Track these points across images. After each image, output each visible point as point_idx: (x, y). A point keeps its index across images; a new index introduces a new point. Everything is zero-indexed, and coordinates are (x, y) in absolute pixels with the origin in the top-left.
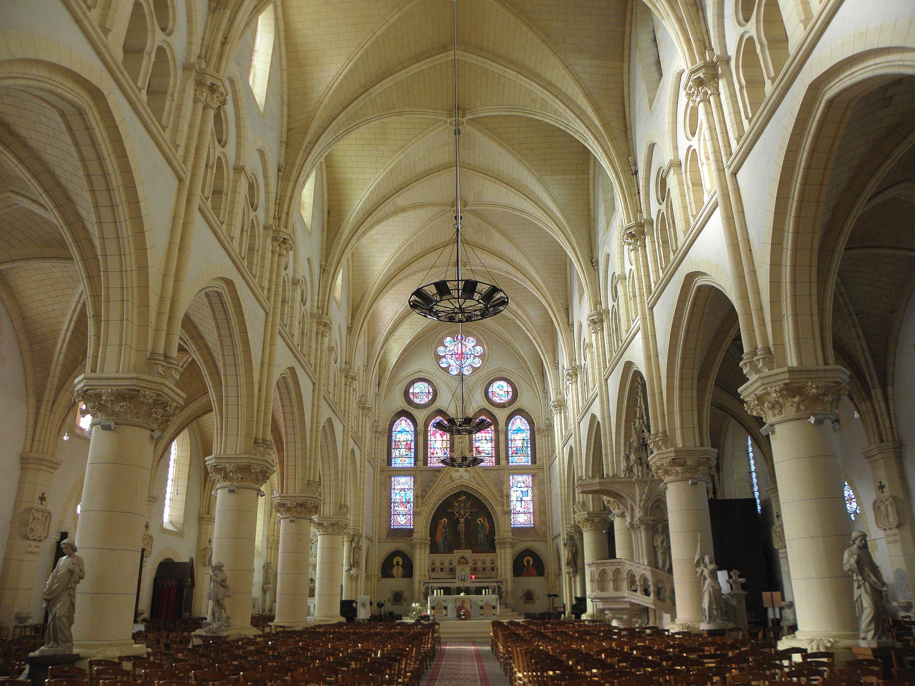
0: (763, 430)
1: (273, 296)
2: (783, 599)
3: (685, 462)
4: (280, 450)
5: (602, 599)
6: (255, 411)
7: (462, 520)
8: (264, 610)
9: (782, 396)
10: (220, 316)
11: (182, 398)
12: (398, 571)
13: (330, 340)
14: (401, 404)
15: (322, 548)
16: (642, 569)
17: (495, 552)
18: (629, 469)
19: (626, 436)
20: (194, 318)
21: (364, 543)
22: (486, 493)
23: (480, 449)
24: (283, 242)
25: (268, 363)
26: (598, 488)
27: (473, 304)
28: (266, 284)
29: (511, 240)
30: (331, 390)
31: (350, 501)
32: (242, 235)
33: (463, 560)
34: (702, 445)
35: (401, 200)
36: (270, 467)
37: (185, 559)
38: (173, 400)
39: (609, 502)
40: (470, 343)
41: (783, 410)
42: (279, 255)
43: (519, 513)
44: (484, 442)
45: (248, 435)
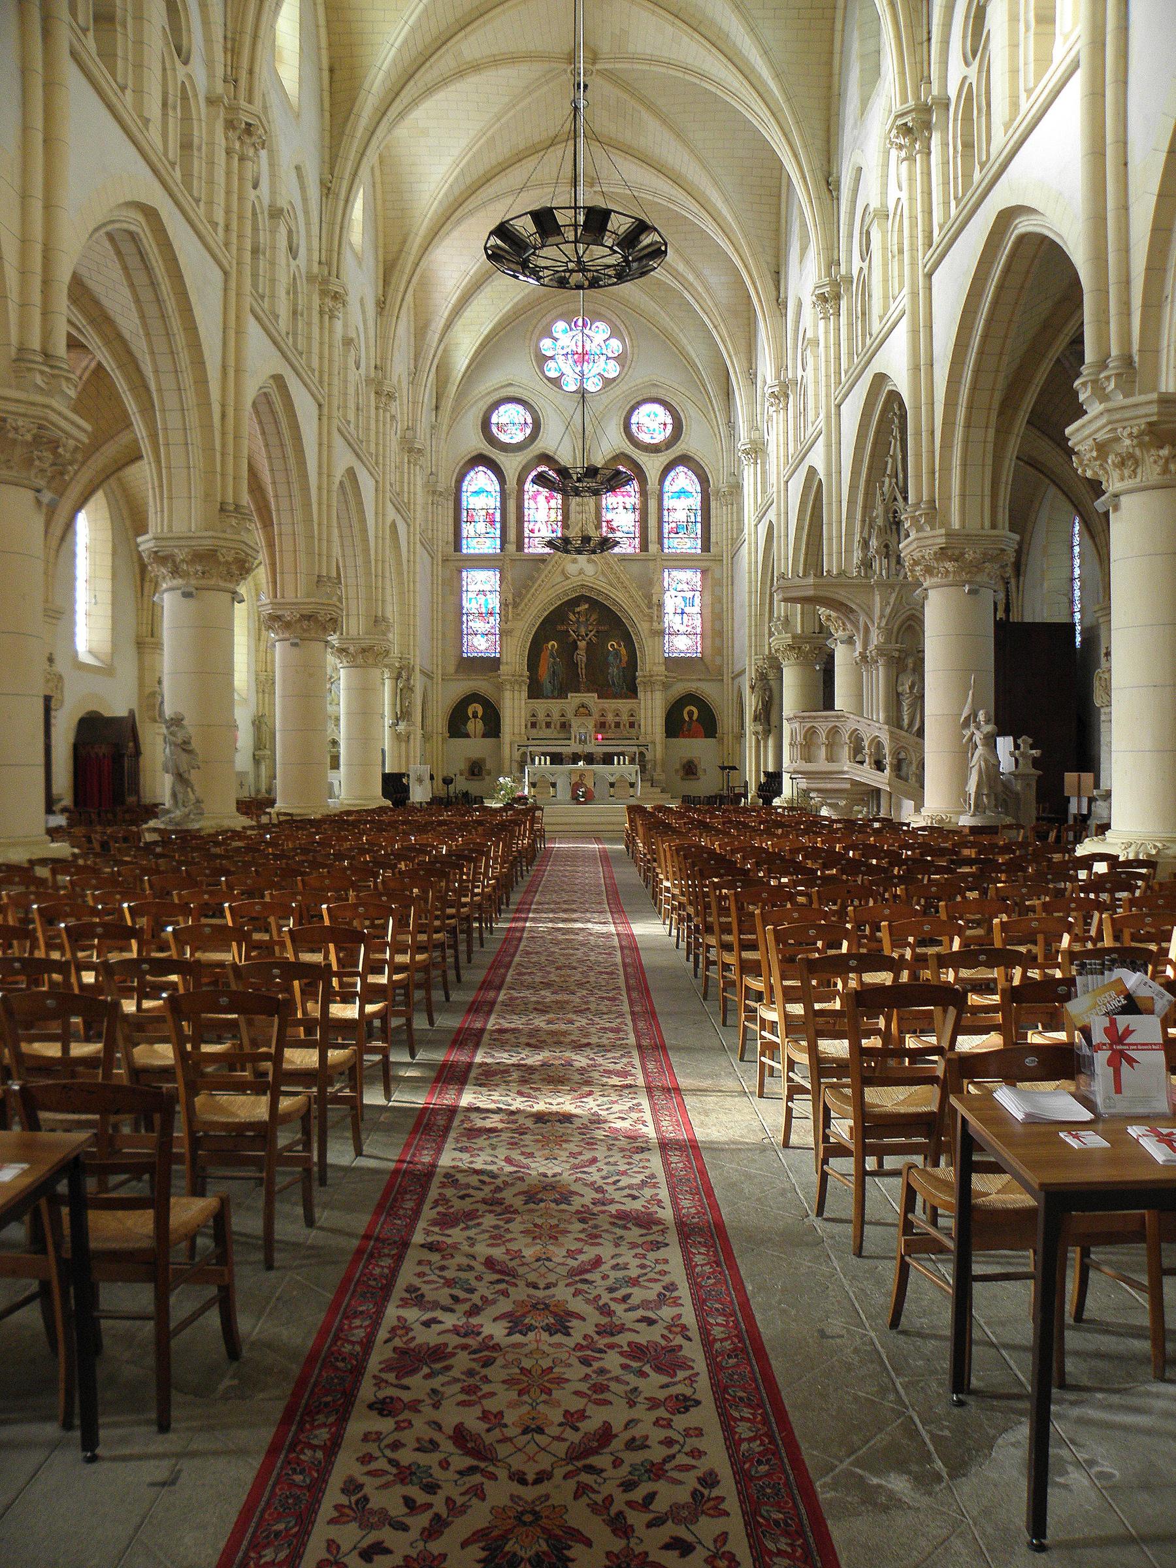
0: (1100, 504)
1: (234, 240)
2: (1097, 785)
3: (963, 554)
4: (267, 523)
5: (807, 774)
6: (218, 456)
7: (582, 644)
8: (258, 791)
9: (1141, 445)
10: (141, 278)
11: (85, 431)
12: (475, 726)
13: (345, 326)
14: (477, 443)
15: (349, 688)
16: (875, 727)
17: (636, 697)
18: (867, 564)
19: (865, 507)
20: (91, 284)
21: (418, 681)
22: (622, 599)
23: (615, 524)
24: (247, 132)
25: (234, 368)
26: (811, 593)
27: (603, 255)
28: (220, 216)
29: (679, 135)
30: (351, 416)
31: (392, 611)
32: (165, 115)
33: (583, 710)
34: (994, 526)
35: (471, 46)
36: (249, 551)
37: (121, 712)
38: (69, 435)
39: (828, 618)
40: (600, 332)
41: (1139, 470)
42: (242, 159)
43: (677, 633)
44: (620, 512)
45: (208, 496)
